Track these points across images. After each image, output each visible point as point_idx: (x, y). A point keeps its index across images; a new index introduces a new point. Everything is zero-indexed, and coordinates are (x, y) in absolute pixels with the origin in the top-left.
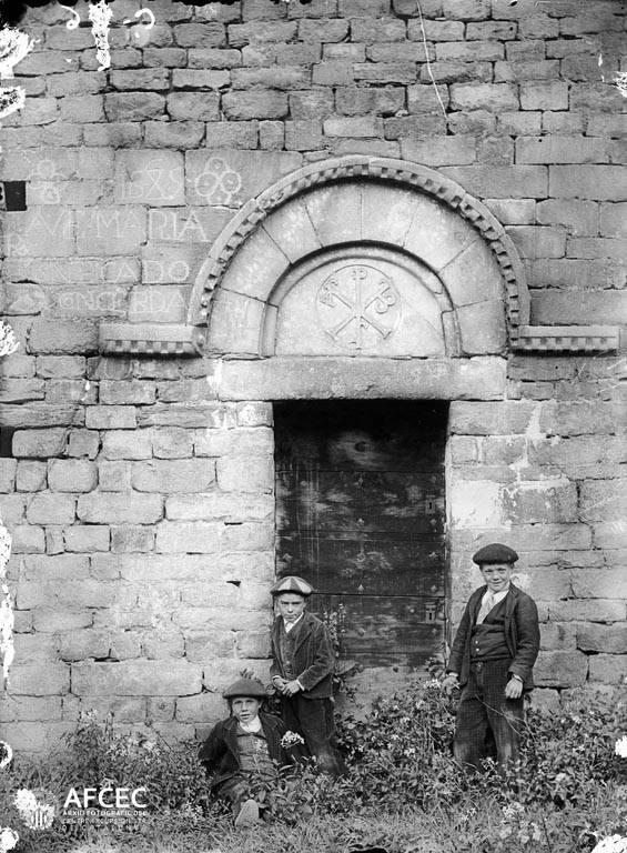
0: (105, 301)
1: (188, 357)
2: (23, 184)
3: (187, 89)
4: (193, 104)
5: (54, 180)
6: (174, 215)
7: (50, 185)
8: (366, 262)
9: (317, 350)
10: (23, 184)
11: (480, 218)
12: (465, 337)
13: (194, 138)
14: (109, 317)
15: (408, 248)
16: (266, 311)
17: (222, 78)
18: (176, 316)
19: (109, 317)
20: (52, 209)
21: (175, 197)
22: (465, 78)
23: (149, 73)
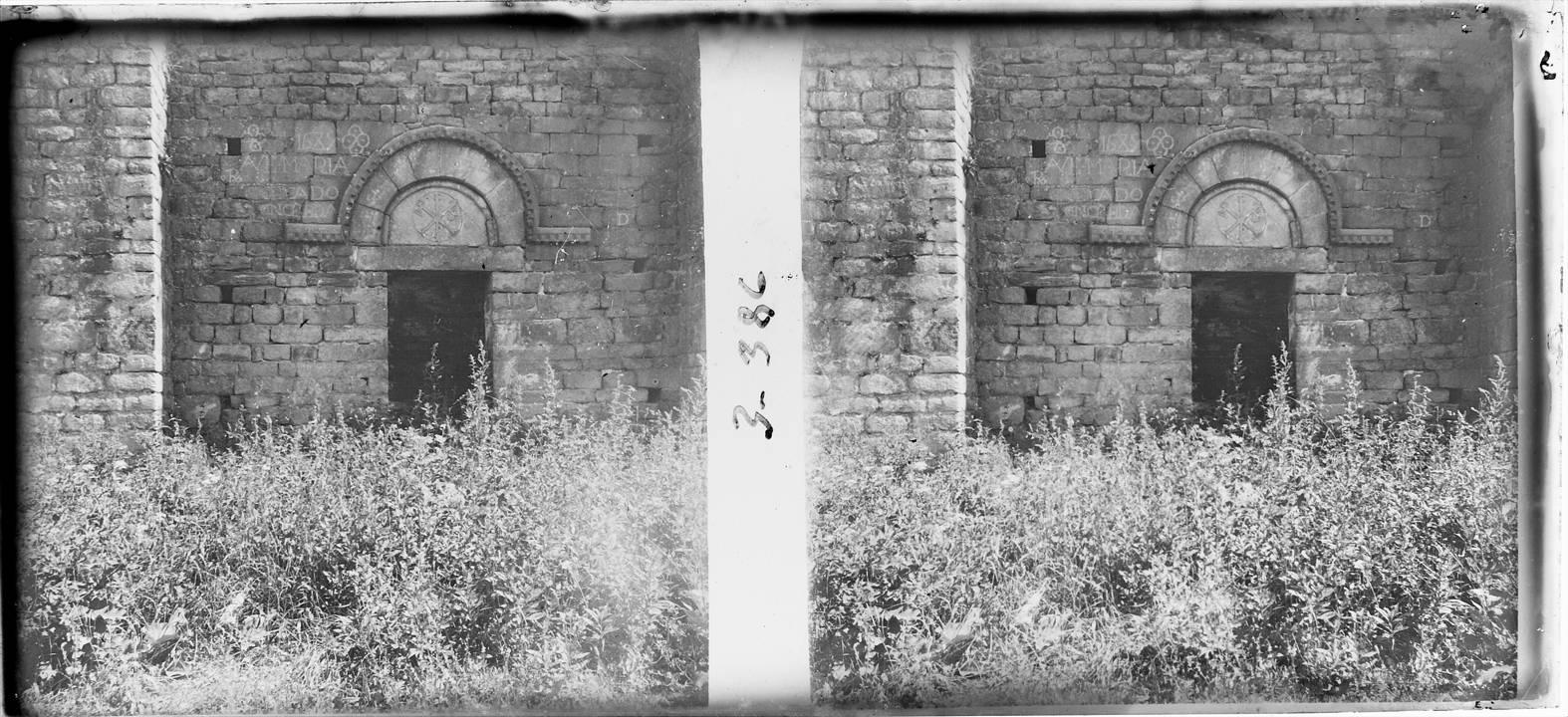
0: (1092, 212)
1: (338, 243)
2: (239, 140)
3: (1142, 87)
4: (1146, 97)
5: (257, 137)
6: (1134, 162)
7: (1060, 142)
8: (441, 190)
9: (413, 242)
10: (239, 140)
11: (511, 163)
12: (1305, 236)
13: (1146, 116)
14: (292, 220)
15: (467, 181)
16: (1188, 219)
17: (359, 78)
18: (331, 220)
19: (292, 220)
20: (256, 155)
21: (330, 148)
22: (502, 82)
23: (315, 76)
